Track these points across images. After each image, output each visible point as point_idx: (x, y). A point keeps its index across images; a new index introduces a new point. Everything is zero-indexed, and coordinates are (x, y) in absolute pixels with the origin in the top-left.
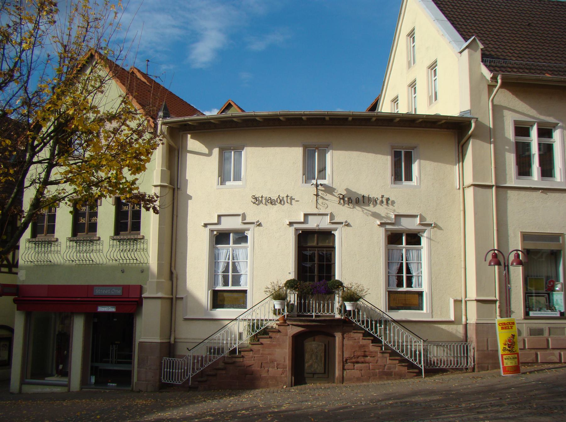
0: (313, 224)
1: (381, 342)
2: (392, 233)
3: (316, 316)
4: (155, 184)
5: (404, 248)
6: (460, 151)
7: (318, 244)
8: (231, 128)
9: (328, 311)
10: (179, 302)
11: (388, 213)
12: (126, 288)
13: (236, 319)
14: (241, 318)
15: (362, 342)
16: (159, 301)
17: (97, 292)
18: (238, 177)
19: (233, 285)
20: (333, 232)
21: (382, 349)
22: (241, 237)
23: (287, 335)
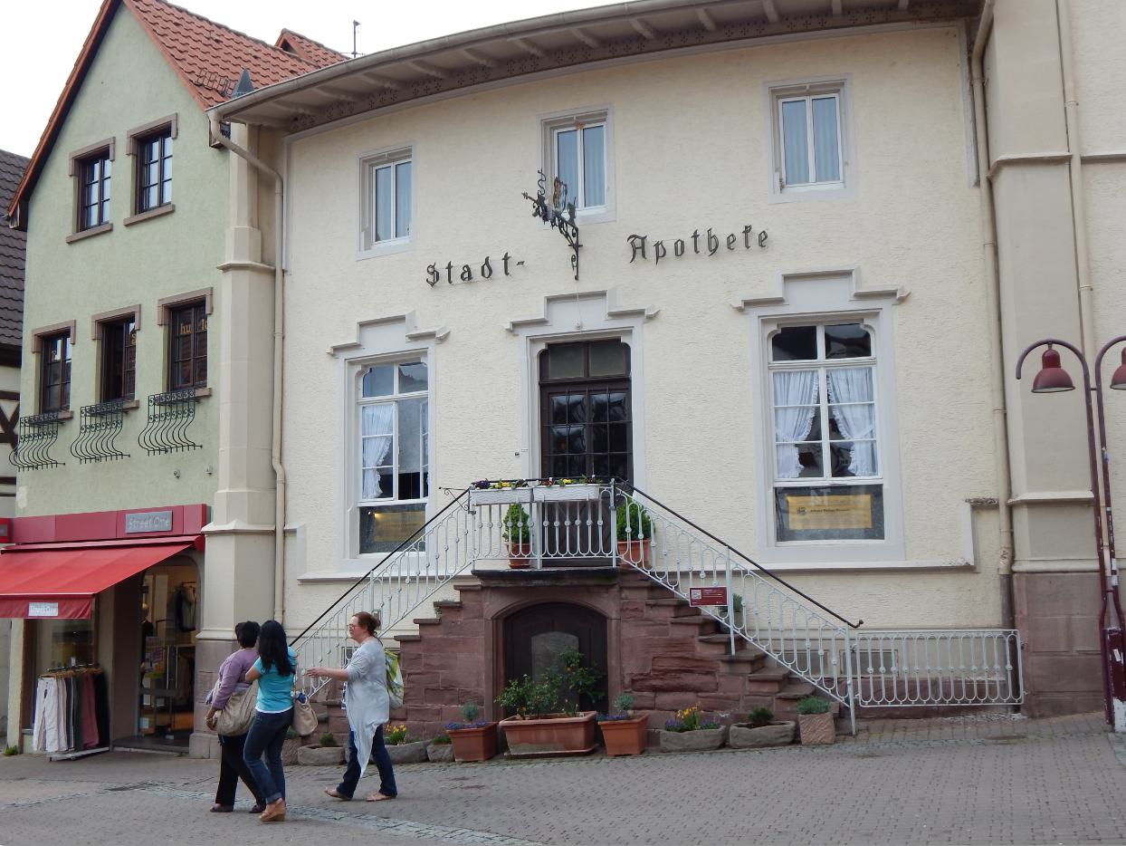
0: (567, 323)
1: (727, 631)
2: (549, 345)
3: (545, 563)
4: (230, 260)
5: (819, 366)
6: (976, 73)
7: (587, 372)
8: (870, 23)
9: (563, 550)
10: (290, 539)
11: (760, 276)
12: (177, 513)
13: (365, 579)
14: (376, 573)
15: (678, 633)
16: (231, 541)
17: (132, 526)
18: (828, 171)
19: (401, 497)
20: (623, 340)
21: (729, 651)
22: (853, 343)
23: (481, 616)
